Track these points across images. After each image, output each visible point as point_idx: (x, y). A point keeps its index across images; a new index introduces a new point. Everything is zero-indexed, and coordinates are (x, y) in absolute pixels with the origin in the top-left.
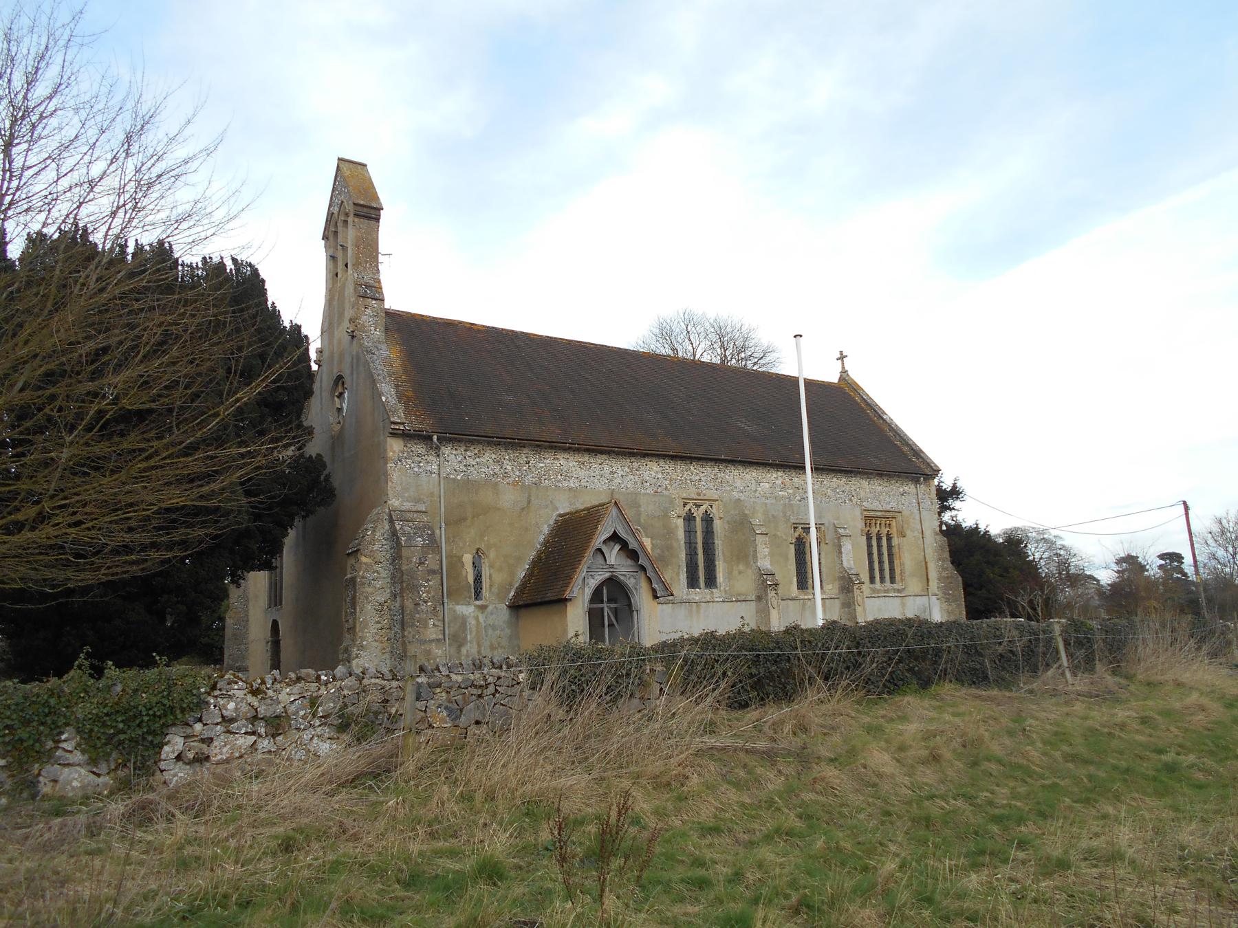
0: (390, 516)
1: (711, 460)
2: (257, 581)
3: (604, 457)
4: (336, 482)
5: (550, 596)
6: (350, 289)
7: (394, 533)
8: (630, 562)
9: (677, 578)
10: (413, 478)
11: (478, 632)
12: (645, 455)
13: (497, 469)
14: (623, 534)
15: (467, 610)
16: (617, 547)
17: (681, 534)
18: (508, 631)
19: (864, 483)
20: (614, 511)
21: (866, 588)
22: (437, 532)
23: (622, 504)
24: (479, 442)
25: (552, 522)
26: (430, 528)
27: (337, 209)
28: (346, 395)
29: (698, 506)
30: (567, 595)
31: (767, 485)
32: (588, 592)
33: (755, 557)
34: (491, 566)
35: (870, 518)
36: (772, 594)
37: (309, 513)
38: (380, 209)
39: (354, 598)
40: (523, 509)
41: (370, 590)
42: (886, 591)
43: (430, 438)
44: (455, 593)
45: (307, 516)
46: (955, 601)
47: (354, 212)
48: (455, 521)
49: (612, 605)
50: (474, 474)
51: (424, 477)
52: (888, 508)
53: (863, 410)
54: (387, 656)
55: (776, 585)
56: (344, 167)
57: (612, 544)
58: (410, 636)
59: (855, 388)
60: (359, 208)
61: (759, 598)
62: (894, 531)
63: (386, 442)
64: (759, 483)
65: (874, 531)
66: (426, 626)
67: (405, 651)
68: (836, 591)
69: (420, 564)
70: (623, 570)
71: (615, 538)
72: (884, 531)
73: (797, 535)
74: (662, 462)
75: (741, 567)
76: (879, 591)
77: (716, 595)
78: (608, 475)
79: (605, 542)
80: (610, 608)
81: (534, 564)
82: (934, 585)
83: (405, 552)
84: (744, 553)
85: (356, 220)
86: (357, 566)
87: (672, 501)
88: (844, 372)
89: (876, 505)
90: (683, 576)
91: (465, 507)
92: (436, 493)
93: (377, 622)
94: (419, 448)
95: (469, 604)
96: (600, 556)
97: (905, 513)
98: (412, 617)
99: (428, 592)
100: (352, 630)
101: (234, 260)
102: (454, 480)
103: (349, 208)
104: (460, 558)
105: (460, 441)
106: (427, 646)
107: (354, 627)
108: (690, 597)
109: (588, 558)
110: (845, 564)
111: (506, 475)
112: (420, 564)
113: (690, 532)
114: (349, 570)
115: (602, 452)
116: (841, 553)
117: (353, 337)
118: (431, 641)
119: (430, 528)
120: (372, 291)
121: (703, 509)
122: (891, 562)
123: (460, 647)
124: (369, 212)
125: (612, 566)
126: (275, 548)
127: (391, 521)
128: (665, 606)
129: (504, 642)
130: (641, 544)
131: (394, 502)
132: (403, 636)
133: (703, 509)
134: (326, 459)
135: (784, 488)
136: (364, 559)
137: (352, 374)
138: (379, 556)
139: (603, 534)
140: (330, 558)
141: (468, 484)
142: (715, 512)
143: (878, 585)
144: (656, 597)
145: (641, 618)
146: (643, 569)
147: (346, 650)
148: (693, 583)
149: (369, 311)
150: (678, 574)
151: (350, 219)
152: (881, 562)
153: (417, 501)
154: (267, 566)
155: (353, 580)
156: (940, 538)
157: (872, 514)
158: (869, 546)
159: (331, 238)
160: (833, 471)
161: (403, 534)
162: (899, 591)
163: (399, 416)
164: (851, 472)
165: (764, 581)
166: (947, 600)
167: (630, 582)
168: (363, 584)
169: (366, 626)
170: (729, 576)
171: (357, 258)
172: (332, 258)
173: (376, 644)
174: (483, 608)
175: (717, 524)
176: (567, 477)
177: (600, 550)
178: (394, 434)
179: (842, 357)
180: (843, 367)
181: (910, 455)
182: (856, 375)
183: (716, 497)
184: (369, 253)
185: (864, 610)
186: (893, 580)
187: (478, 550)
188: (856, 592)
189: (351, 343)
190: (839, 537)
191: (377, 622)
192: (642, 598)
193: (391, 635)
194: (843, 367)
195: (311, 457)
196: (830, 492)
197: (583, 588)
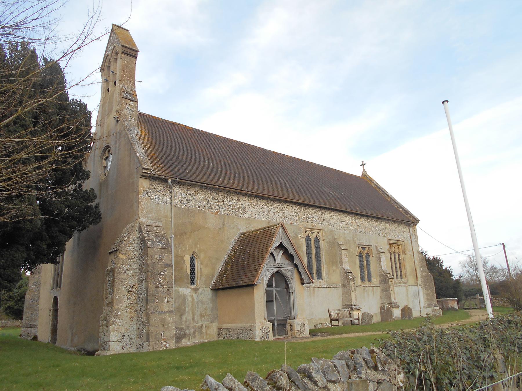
0: (140, 228)
2: (47, 269)
4: (102, 209)
5: (242, 282)
6: (117, 94)
7: (143, 240)
8: (288, 262)
10: (156, 206)
11: (193, 305)
12: (286, 202)
14: (286, 244)
15: (186, 291)
16: (281, 252)
18: (211, 305)
19: (387, 225)
20: (281, 230)
23: (286, 227)
25: (237, 238)
26: (165, 237)
27: (110, 52)
28: (111, 158)
29: (312, 232)
33: (341, 262)
34: (201, 264)
36: (351, 283)
37: (85, 227)
39: (113, 282)
40: (220, 229)
42: (400, 283)
43: (166, 181)
44: (178, 280)
45: (82, 230)
46: (430, 289)
47: (122, 51)
48: (180, 234)
49: (277, 289)
50: (192, 206)
51: (161, 205)
54: (134, 322)
55: (354, 278)
57: (278, 250)
58: (152, 309)
59: (371, 180)
60: (124, 49)
61: (344, 286)
63: (138, 181)
66: (162, 302)
67: (148, 319)
69: (160, 260)
71: (281, 246)
72: (397, 250)
74: (294, 206)
75: (334, 268)
77: (322, 284)
78: (266, 212)
80: (277, 291)
81: (227, 263)
83: (150, 252)
84: (336, 261)
85: (123, 55)
86: (116, 260)
87: (299, 229)
88: (364, 172)
89: (393, 237)
91: (187, 226)
93: (128, 299)
94: (159, 186)
95: (187, 287)
97: (406, 242)
98: (154, 295)
99: (164, 279)
100: (110, 304)
102: (180, 208)
103: (119, 49)
104: (183, 257)
105: (184, 184)
106: (163, 316)
107: (112, 302)
109: (268, 259)
110: (383, 268)
111: (211, 208)
112: (160, 260)
113: (308, 247)
116: (380, 261)
117: (118, 121)
118: (166, 312)
119: (165, 237)
120: (131, 97)
121: (315, 234)
123: (181, 315)
124: (132, 53)
126: (61, 250)
127: (140, 231)
129: (209, 312)
131: (143, 220)
132: (147, 309)
133: (315, 234)
134: (97, 192)
135: (352, 225)
136: (121, 256)
137: (116, 143)
138: (131, 255)
140: (97, 256)
141: (188, 211)
142: (320, 236)
144: (303, 284)
146: (296, 266)
147: (105, 318)
149: (128, 107)
152: (396, 268)
153: (158, 220)
154: (53, 261)
155: (113, 270)
158: (361, 262)
159: (106, 70)
161: (149, 240)
162: (405, 283)
163: (148, 165)
166: (426, 288)
167: (289, 274)
168: (120, 273)
170: (329, 274)
171: (123, 77)
172: (106, 81)
173: (126, 314)
174: (196, 290)
175: (322, 244)
177: (272, 254)
178: (143, 176)
179: (363, 165)
180: (364, 169)
181: (403, 212)
183: (321, 228)
184: (130, 75)
185: (394, 292)
187: (194, 253)
189: (116, 125)
190: (379, 253)
191: (128, 299)
192: (295, 284)
193: (138, 308)
195: (86, 190)
196: (373, 229)
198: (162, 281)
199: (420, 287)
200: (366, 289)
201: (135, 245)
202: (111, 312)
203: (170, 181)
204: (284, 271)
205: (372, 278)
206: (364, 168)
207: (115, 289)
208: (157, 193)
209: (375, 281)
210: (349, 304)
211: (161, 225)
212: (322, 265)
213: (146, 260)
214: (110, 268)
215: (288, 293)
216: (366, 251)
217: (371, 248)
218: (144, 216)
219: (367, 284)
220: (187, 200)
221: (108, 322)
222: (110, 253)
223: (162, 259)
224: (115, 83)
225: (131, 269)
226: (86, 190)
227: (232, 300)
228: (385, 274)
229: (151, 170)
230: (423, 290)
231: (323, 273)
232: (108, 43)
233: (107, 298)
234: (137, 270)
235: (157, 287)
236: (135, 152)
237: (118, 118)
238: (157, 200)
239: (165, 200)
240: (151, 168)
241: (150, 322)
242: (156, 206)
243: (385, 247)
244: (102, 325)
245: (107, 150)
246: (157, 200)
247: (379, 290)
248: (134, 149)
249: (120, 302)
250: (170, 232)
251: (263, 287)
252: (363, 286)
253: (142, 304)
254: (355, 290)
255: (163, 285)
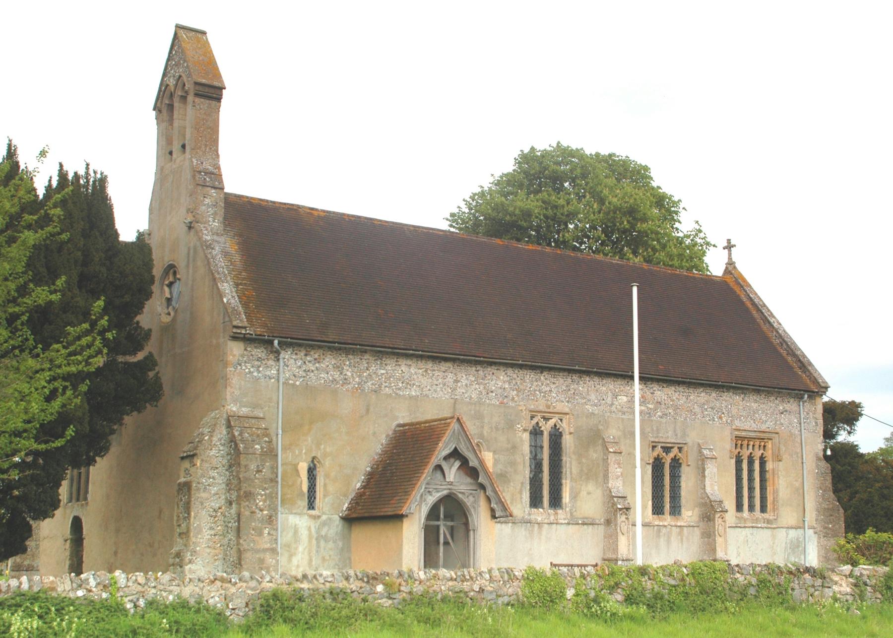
1: (564, 370)
3: (449, 364)
5: (389, 511)
9: (517, 497)
13: (337, 375)
16: (457, 464)
17: (526, 449)
20: (454, 426)
21: (731, 515)
22: (274, 439)
24: (320, 347)
29: (546, 419)
30: (404, 511)
31: (625, 399)
32: (425, 510)
33: (606, 477)
34: (327, 476)
35: (743, 438)
36: (621, 518)
38: (222, 88)
41: (204, 495)
43: (271, 343)
47: (190, 89)
49: (450, 523)
52: (764, 427)
53: (747, 310)
55: (628, 509)
56: (181, 33)
57: (452, 460)
61: (608, 522)
62: (769, 454)
63: (226, 345)
64: (615, 396)
65: (745, 453)
66: (261, 534)
67: (240, 559)
68: (695, 518)
69: (259, 471)
70: (463, 488)
71: (455, 454)
72: (758, 453)
73: (655, 454)
74: (510, 371)
76: (745, 520)
78: (451, 384)
79: (446, 458)
82: (811, 516)
85: (197, 100)
86: (192, 470)
88: (731, 263)
90: (526, 496)
92: (275, 398)
94: (259, 352)
96: (439, 475)
100: (185, 534)
101: (102, 174)
105: (300, 345)
106: (261, 555)
108: (532, 517)
110: (708, 490)
111: (346, 381)
113: (536, 448)
114: (182, 474)
115: (446, 360)
116: (704, 476)
117: (190, 228)
120: (214, 178)
121: (551, 423)
122: (763, 488)
124: (212, 92)
125: (451, 483)
127: (229, 426)
128: (503, 525)
130: (481, 462)
131: (233, 408)
132: (238, 544)
133: (551, 423)
137: (188, 266)
139: (443, 449)
141: (308, 390)
142: (565, 426)
143: (746, 513)
144: (494, 517)
145: (477, 536)
146: (482, 487)
147: (178, 555)
148: (535, 501)
149: (207, 201)
150: (521, 492)
151: (190, 98)
152: (751, 489)
156: (824, 464)
157: (744, 434)
159: (164, 111)
160: (702, 385)
161: (242, 441)
162: (769, 521)
163: (242, 320)
164: (723, 387)
165: (614, 504)
167: (468, 501)
168: (198, 489)
169: (200, 531)
170: (575, 497)
173: (208, 550)
175: (568, 441)
176: (409, 384)
177: (439, 468)
178: (235, 338)
180: (730, 258)
182: (745, 269)
183: (567, 410)
185: (726, 541)
186: (763, 509)
187: (314, 458)
188: (718, 521)
192: (480, 517)
194: (730, 258)
196: (697, 409)
197: (420, 505)
198: (261, 503)
199: (810, 532)
200: (664, 530)
201: (221, 448)
202: (185, 545)
203: (276, 342)
204: (460, 496)
205: (683, 510)
206: (730, 254)
207: (192, 514)
208: (256, 363)
209: (689, 514)
210: (614, 556)
211: (262, 416)
212: (564, 481)
213: (238, 472)
214: (182, 480)
215: (467, 530)
216: (672, 455)
217: (685, 448)
218: (235, 401)
219: (667, 519)
220: (305, 371)
221: (182, 560)
222: (183, 458)
223: (261, 471)
224: (184, 146)
225: (216, 484)
226: (49, 188)
227: (367, 537)
228: (711, 501)
229: (245, 328)
230: (819, 538)
231: (564, 495)
232: (168, 60)
233: (179, 526)
234: (224, 486)
235: (253, 512)
236: (221, 295)
237: (191, 223)
238: (255, 374)
239: (268, 373)
240: (246, 324)
241: (243, 563)
242: (255, 384)
243: (721, 447)
244: (173, 565)
245: (172, 271)
246: (255, 374)
247: (697, 532)
248: (218, 288)
249: (198, 533)
250: (275, 425)
251: (420, 520)
252: (656, 523)
253: (232, 536)
254: (628, 532)
255: (261, 510)
